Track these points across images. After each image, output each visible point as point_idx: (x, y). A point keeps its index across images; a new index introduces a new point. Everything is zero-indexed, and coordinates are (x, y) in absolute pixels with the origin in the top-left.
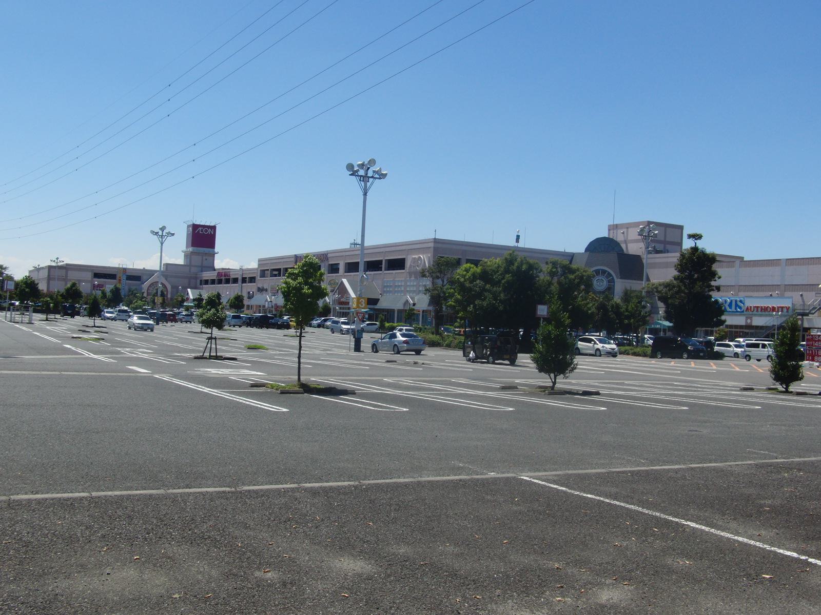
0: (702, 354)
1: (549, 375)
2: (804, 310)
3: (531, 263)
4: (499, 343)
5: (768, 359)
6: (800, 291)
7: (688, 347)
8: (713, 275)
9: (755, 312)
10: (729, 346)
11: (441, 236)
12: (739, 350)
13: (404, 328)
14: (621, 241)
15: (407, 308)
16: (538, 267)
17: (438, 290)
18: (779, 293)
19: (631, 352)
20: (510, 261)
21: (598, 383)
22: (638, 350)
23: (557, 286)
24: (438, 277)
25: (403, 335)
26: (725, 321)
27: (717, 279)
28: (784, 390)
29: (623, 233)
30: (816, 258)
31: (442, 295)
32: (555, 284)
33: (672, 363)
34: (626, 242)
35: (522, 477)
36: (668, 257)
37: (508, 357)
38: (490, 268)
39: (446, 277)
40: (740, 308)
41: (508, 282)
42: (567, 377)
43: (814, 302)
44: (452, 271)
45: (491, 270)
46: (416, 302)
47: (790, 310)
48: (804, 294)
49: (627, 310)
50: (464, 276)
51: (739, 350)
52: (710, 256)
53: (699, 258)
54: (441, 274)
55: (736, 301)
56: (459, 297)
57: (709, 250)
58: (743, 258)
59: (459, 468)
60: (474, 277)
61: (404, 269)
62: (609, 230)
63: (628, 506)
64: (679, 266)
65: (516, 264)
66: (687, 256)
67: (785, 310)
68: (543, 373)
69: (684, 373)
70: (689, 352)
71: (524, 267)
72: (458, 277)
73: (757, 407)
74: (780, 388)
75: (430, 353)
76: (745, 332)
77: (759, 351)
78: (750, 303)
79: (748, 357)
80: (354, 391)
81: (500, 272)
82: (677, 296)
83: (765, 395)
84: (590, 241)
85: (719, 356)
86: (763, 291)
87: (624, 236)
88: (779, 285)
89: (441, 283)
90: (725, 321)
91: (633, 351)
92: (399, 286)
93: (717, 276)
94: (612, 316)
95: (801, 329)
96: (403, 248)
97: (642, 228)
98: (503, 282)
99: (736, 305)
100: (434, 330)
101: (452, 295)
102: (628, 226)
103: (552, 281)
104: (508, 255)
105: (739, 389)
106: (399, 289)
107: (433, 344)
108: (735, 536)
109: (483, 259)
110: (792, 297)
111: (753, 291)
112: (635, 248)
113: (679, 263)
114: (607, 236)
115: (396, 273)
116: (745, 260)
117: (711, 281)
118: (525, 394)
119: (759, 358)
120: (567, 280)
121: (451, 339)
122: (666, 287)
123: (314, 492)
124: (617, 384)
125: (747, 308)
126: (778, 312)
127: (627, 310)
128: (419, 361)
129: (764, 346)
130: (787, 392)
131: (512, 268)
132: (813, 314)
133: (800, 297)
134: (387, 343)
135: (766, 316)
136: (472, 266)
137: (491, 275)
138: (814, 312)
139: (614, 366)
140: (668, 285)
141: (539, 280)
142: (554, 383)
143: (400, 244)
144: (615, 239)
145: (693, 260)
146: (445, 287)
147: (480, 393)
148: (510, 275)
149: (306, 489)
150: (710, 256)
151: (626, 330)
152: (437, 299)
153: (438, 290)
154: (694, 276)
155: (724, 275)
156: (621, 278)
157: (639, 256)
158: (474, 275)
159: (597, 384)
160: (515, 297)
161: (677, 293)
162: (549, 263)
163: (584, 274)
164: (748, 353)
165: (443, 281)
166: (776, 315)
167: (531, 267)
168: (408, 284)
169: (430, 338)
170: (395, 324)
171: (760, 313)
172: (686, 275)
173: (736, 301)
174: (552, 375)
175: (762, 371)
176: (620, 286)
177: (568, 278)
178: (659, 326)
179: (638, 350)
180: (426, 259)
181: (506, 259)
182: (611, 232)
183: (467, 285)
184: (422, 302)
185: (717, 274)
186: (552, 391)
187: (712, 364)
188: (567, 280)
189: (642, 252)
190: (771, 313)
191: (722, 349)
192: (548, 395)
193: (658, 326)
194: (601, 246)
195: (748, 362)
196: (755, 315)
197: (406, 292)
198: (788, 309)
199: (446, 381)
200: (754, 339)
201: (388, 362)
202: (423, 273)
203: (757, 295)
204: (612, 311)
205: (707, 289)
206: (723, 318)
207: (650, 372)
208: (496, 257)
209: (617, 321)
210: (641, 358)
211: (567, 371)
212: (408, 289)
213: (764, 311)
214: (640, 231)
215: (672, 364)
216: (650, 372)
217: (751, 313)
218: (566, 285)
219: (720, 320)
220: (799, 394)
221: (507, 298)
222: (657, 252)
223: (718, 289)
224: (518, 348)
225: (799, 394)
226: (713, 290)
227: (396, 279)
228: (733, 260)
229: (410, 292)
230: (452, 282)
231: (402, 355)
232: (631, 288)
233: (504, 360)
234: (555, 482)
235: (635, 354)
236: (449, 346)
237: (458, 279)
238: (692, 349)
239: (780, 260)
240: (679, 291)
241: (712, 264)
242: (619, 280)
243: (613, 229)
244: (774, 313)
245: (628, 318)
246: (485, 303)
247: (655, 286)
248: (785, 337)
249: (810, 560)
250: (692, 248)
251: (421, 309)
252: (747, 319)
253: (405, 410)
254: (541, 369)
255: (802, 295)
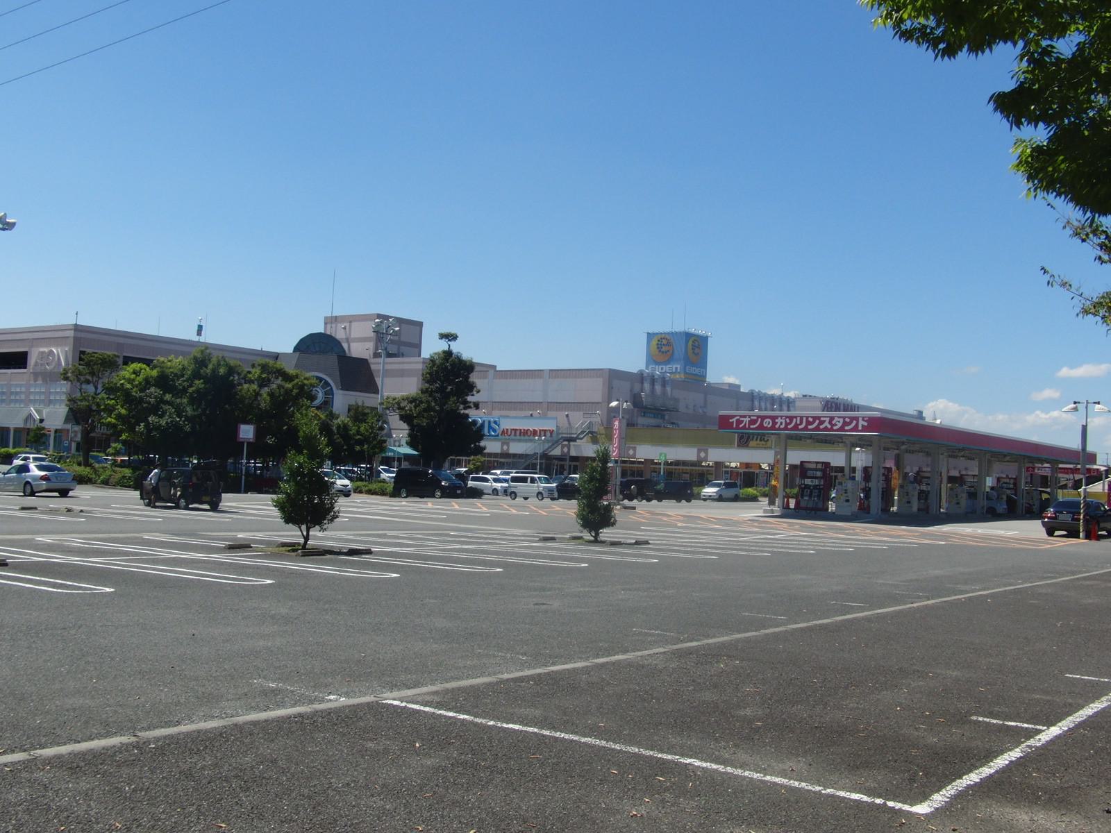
0: (459, 492)
1: (300, 527)
2: (571, 434)
3: (232, 365)
4: (194, 480)
5: (537, 497)
6: (565, 411)
7: (441, 482)
8: (471, 388)
9: (512, 437)
10: (486, 480)
11: (86, 321)
12: (498, 485)
13: (31, 456)
14: (341, 339)
15: (31, 426)
16: (242, 372)
17: (88, 401)
18: (541, 412)
19: (364, 489)
20: (201, 361)
21: (354, 535)
22: (374, 486)
23: (268, 398)
24: (88, 382)
25: (41, 468)
26: (484, 448)
27: (475, 393)
28: (592, 538)
29: (345, 328)
30: (585, 370)
31: (94, 408)
32: (265, 396)
33: (429, 505)
34: (348, 340)
35: (384, 702)
36: (403, 363)
37: (208, 499)
38: (171, 370)
39: (100, 381)
40: (495, 431)
41: (198, 391)
42: (325, 529)
43: (582, 424)
44: (111, 373)
45: (172, 373)
46: (44, 417)
47: (554, 435)
48: (571, 414)
49: (358, 433)
50: (130, 381)
51: (498, 485)
52: (468, 364)
53: (453, 365)
54: (92, 377)
55: (489, 422)
56: (123, 411)
57: (466, 356)
58: (495, 367)
59: (266, 693)
60: (147, 382)
61: (25, 368)
62: (326, 324)
63: (572, 737)
64: (428, 375)
65: (210, 366)
66: (437, 362)
67: (548, 434)
68: (290, 525)
69: (451, 518)
70: (443, 489)
71: (222, 371)
72: (121, 382)
73: (583, 565)
74: (588, 536)
75: (83, 494)
76: (500, 462)
77: (527, 486)
78: (507, 424)
79: (514, 495)
80: (5, 560)
81: (186, 376)
82: (426, 415)
83: (572, 547)
84: (301, 337)
85: (476, 494)
86: (521, 409)
87: (346, 333)
88: (542, 403)
89: (93, 389)
90: (484, 448)
91: (367, 488)
92: (17, 393)
93: (475, 389)
94: (338, 441)
95: (568, 458)
96: (25, 336)
97: (378, 322)
98: (190, 390)
99: (490, 427)
100: (81, 459)
101: (110, 410)
102: (352, 319)
103: (260, 391)
104: (198, 353)
105: (537, 539)
106: (18, 398)
107: (82, 480)
108: (820, 791)
109: (158, 358)
110: (556, 418)
111: (510, 409)
112: (360, 350)
113: (428, 371)
114: (323, 332)
115: (12, 373)
116: (498, 369)
117: (467, 395)
118: (266, 557)
119: (526, 495)
120: (282, 390)
121: (108, 473)
122: (411, 402)
123: (72, 766)
124: (379, 536)
125: (503, 431)
126: (540, 436)
127: (358, 433)
128: (74, 507)
129: (533, 480)
130: (596, 541)
131: (205, 372)
132: (581, 439)
133: (565, 419)
134: (13, 479)
135: (526, 441)
136: (144, 366)
137: (173, 380)
138: (582, 436)
139: (355, 509)
140: (412, 400)
141: (241, 390)
142: (307, 538)
143: (53, 329)
144: (333, 335)
145: (446, 367)
146: (100, 396)
147: (200, 556)
148: (202, 381)
149: (49, 761)
150: (468, 364)
151: (357, 459)
152: (77, 414)
153: (88, 401)
154: (446, 388)
155: (484, 390)
156: (341, 389)
157: (366, 360)
158: (147, 380)
159: (352, 537)
160: (208, 412)
161: (425, 410)
162: (256, 365)
163: (306, 382)
164: (513, 490)
165: (96, 388)
166: (538, 440)
167: (231, 370)
168: (32, 390)
169: (76, 471)
170: (11, 450)
171: (518, 437)
172: (437, 387)
173: (489, 422)
174: (304, 527)
175: (545, 514)
176: (342, 401)
177: (283, 388)
178: (392, 454)
179: (374, 486)
180: (62, 354)
181: (195, 358)
182: (329, 326)
183: (135, 393)
184: (55, 416)
185: (475, 387)
186: (305, 551)
187: (454, 503)
188: (282, 390)
189: (370, 355)
190: (532, 437)
191: (478, 485)
192: (302, 556)
193: (390, 454)
194: (314, 345)
195: (541, 502)
196: (514, 440)
197: (28, 402)
198: (552, 432)
199: (137, 538)
200: (514, 471)
201: (23, 509)
202: (65, 374)
203: (514, 415)
204: (338, 433)
205: (461, 407)
206: (482, 444)
207: (423, 519)
208: (177, 354)
209: (345, 447)
210: (378, 497)
211: (325, 522)
212: (32, 398)
213: (524, 435)
214: (376, 326)
215: (430, 505)
216: (423, 519)
217: (507, 437)
218: (281, 398)
219: (479, 446)
220: (613, 544)
221: (196, 413)
222: (389, 355)
223: (477, 406)
224: (222, 485)
225: (613, 544)
226: (470, 407)
227: (12, 383)
228: (485, 369)
229: (34, 402)
230: (111, 390)
231: (38, 498)
232: (363, 403)
233: (202, 503)
234: (439, 705)
235: (370, 492)
236: (106, 483)
237: (122, 384)
238: (447, 485)
239: (543, 370)
240: (428, 409)
241: (470, 374)
242: (341, 392)
243: (332, 323)
244: (537, 438)
245: (360, 443)
246: (163, 422)
247: (396, 401)
248: (594, 471)
249: (890, 804)
250: (444, 352)
251: (53, 428)
252: (699, 451)
253: (108, 590)
254: (288, 519)
255: (567, 416)
